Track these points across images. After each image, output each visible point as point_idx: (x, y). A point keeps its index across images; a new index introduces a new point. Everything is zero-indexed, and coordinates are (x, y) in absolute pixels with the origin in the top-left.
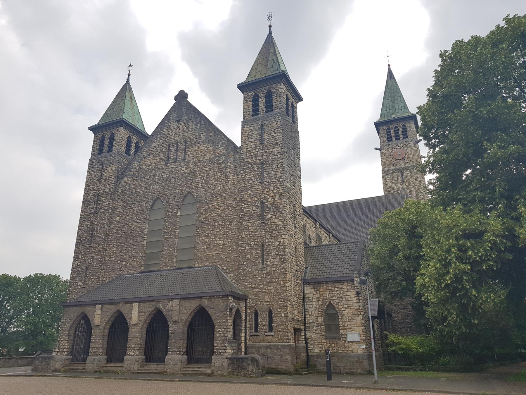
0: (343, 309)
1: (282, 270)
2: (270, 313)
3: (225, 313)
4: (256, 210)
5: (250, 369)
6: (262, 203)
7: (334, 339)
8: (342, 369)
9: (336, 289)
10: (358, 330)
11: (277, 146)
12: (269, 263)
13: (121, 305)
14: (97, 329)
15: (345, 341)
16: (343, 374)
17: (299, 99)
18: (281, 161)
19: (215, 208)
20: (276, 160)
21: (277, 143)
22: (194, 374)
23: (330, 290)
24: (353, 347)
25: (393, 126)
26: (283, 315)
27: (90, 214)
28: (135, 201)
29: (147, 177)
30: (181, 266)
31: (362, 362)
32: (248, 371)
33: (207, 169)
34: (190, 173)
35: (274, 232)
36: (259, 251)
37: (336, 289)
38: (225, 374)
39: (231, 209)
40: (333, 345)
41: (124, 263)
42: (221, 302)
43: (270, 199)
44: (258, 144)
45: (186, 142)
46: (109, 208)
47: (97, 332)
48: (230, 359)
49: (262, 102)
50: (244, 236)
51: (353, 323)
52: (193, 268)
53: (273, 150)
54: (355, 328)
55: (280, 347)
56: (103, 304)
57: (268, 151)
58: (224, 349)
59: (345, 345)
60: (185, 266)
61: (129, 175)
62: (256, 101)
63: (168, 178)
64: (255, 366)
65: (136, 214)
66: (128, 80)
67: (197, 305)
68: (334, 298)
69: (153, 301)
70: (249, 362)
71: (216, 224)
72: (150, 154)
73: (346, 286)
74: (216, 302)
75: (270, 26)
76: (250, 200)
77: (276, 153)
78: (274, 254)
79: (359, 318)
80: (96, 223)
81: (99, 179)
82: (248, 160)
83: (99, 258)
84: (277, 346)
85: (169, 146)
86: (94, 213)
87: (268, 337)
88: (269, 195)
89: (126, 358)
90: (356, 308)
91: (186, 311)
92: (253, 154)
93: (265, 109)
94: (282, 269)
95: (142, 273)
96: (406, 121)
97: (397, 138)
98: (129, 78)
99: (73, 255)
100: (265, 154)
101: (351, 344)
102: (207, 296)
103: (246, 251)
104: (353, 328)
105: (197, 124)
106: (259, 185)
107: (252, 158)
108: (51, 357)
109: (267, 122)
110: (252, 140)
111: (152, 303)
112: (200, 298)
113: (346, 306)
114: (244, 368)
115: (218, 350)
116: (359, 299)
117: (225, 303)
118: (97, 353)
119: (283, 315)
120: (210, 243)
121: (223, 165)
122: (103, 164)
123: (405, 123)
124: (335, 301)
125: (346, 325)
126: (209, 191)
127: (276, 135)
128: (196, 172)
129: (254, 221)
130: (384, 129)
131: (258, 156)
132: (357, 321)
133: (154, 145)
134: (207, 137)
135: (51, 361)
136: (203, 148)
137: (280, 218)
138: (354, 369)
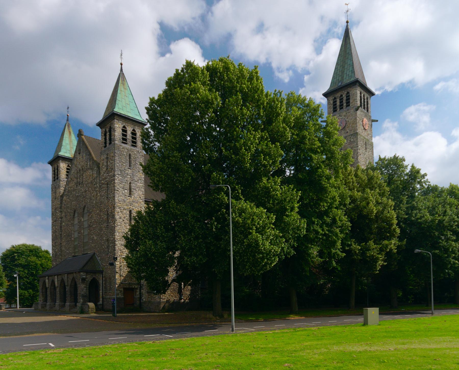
25: (338, 95)
56: (58, 275)
66: (121, 70)
96: (350, 87)
97: (341, 107)
98: (121, 67)
112: (72, 273)
123: (349, 90)
130: (331, 98)
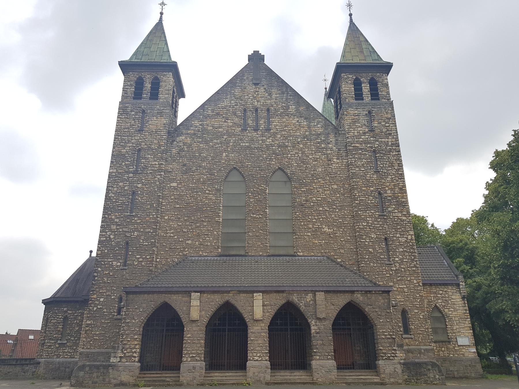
0: (450, 313)
1: (414, 269)
2: (404, 313)
3: (388, 311)
4: (372, 200)
5: (431, 375)
6: (380, 193)
7: (444, 343)
8: (456, 373)
9: (441, 292)
10: (467, 334)
11: (390, 137)
12: (397, 259)
13: (231, 295)
14: (194, 325)
15: (455, 345)
16: (457, 378)
17: (183, 96)
18: (397, 153)
19: (318, 191)
20: (390, 151)
21: (390, 134)
22: (362, 383)
23: (435, 293)
24: (464, 350)
26: (422, 317)
27: (128, 172)
28: (200, 167)
29: (216, 141)
30: (277, 253)
31: (475, 366)
32: (429, 377)
33: (301, 146)
34: (279, 146)
35: (399, 227)
36: (383, 245)
37: (441, 292)
38: (400, 381)
39: (338, 195)
40: (443, 349)
41: (189, 242)
42: (380, 298)
43: (389, 191)
44: (367, 130)
45: (268, 110)
46: (160, 170)
47: (194, 329)
48: (404, 364)
49: (366, 89)
50: (362, 227)
51: (461, 327)
52: (295, 256)
53: (387, 140)
54: (464, 331)
55: (423, 351)
57: (380, 140)
58: (393, 353)
59: (456, 348)
60: (281, 253)
61: (187, 134)
62: (139, 85)
63: (248, 147)
64: (437, 372)
65: (204, 183)
67: (348, 300)
68: (439, 301)
69: (283, 292)
70: (430, 367)
71: (321, 209)
72: (218, 114)
73: (450, 290)
74: (373, 298)
75: (162, 14)
76: (365, 189)
77: (390, 143)
78: (402, 250)
79: (467, 322)
80: (139, 186)
81: (141, 130)
82: (357, 145)
83: (149, 232)
84: (420, 350)
85: (245, 110)
86: (135, 173)
87: (407, 340)
88: (387, 187)
89: (249, 364)
90: (463, 312)
91: (333, 307)
92: (362, 140)
93: (370, 96)
94: (414, 267)
95: (220, 256)
99: (99, 224)
100: (377, 143)
101: (461, 347)
102: (362, 291)
103: (367, 243)
104: (462, 331)
105: (283, 93)
106: (373, 174)
107: (361, 144)
108: (110, 366)
109: (375, 109)
110: (359, 125)
111: (281, 295)
112: (353, 292)
113: (452, 309)
114: (424, 375)
115: (385, 353)
116: (464, 303)
117: (386, 300)
118: (198, 359)
119: (422, 317)
120: (316, 231)
121: (323, 146)
122: (143, 112)
124: (440, 304)
125: (455, 328)
126: (307, 171)
127: (387, 125)
128: (287, 146)
129: (372, 211)
131: (369, 143)
132: (466, 325)
133: (223, 104)
134: (297, 110)
135: (111, 371)
136: (293, 122)
137: (404, 213)
138: (468, 373)
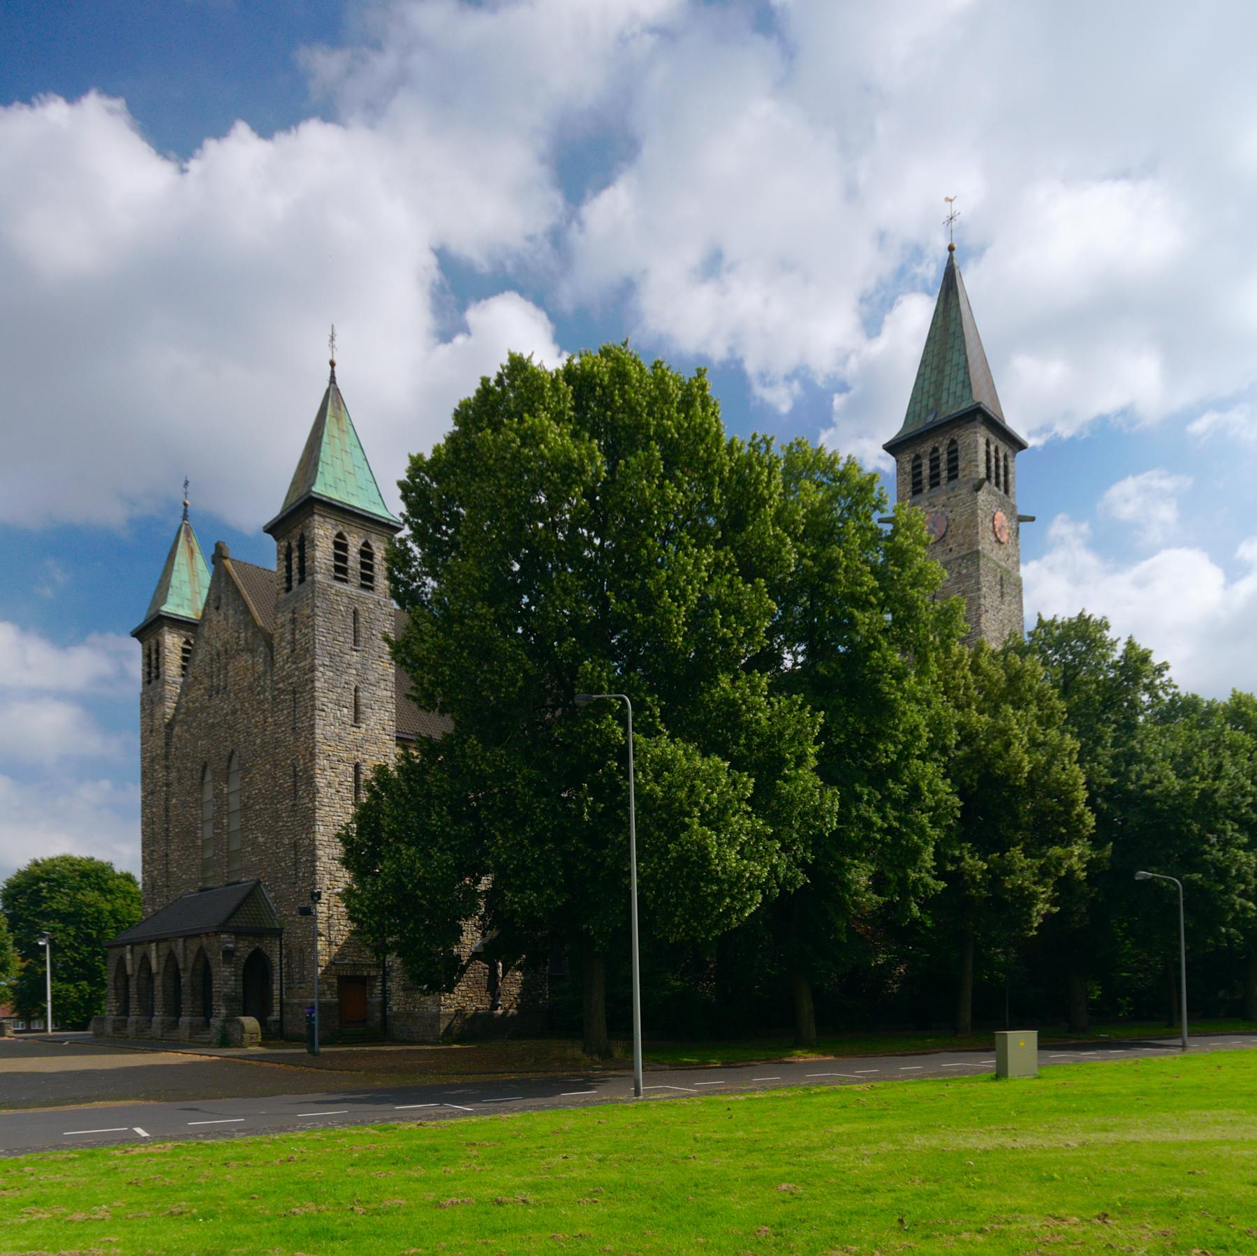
25: (927, 447)
66: (333, 379)
96: (959, 427)
97: (935, 482)
98: (333, 372)
112: (198, 935)
123: (956, 433)
130: (907, 457)
